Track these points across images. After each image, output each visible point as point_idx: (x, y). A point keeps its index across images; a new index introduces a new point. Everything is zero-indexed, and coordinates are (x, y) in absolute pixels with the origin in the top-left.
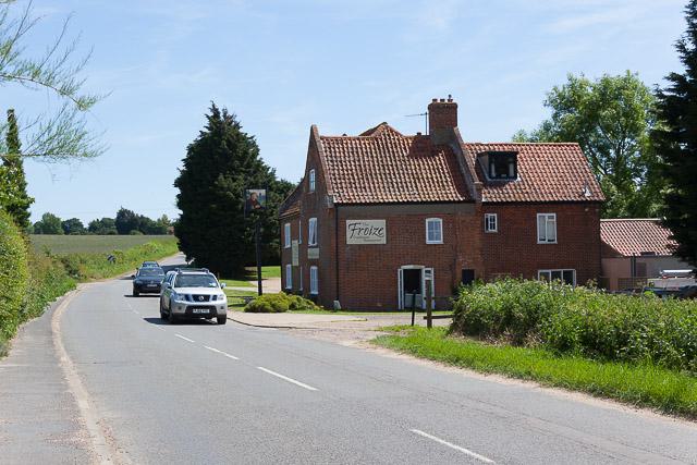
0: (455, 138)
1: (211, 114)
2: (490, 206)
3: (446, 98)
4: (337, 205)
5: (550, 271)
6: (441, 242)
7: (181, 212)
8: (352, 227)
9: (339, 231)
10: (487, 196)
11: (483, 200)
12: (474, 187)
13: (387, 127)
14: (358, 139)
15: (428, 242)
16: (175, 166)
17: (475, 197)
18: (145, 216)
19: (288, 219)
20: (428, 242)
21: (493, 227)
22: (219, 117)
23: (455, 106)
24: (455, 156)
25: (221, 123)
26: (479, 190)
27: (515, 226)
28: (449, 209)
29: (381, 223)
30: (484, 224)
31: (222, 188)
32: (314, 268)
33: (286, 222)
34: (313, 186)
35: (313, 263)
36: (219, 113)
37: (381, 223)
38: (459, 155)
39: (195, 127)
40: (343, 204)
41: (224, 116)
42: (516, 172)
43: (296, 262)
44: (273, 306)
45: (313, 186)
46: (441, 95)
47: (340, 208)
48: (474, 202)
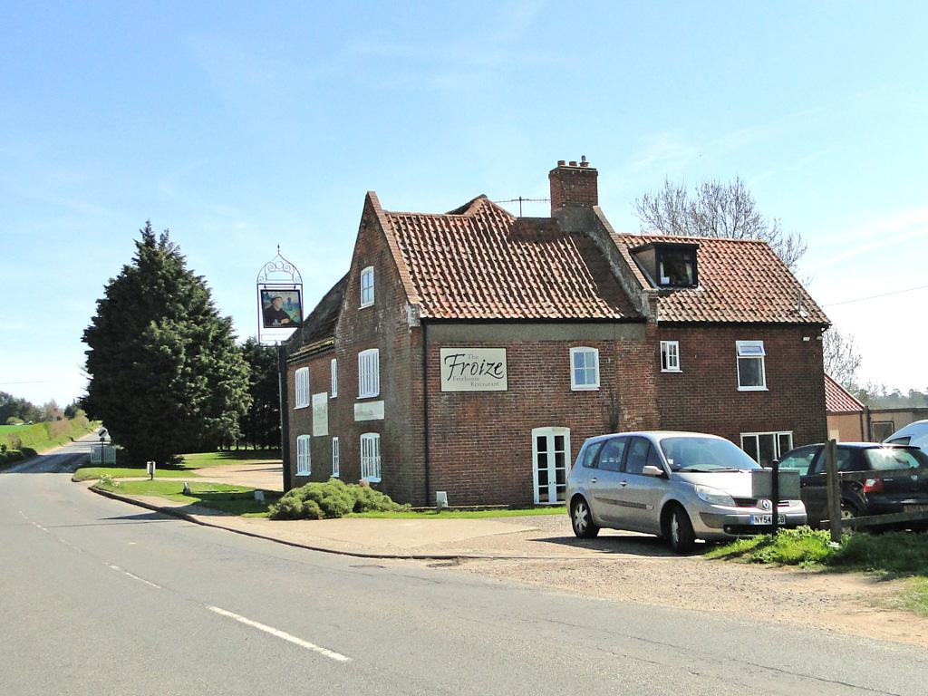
0: (597, 223)
1: (142, 241)
2: (669, 328)
3: (579, 161)
4: (424, 322)
5: (757, 435)
6: (595, 386)
7: (91, 377)
8: (450, 361)
9: (428, 369)
10: (666, 311)
11: (660, 319)
12: (644, 298)
13: (488, 203)
14: (445, 218)
15: (574, 387)
16: (86, 314)
17: (646, 312)
18: (27, 400)
19: (303, 360)
20: (574, 387)
21: (673, 363)
22: (153, 246)
23: (593, 175)
24: (599, 251)
25: (156, 254)
26: (653, 301)
27: (706, 362)
28: (606, 332)
29: (499, 355)
30: (660, 359)
31: (153, 341)
32: (372, 437)
33: (299, 366)
34: (368, 298)
35: (370, 426)
36: (153, 242)
37: (499, 355)
38: (607, 250)
39: (124, 257)
40: (435, 321)
41: (162, 245)
42: (695, 273)
43: (320, 427)
44: (323, 507)
45: (368, 298)
46: (571, 156)
47: (432, 328)
48: (642, 320)
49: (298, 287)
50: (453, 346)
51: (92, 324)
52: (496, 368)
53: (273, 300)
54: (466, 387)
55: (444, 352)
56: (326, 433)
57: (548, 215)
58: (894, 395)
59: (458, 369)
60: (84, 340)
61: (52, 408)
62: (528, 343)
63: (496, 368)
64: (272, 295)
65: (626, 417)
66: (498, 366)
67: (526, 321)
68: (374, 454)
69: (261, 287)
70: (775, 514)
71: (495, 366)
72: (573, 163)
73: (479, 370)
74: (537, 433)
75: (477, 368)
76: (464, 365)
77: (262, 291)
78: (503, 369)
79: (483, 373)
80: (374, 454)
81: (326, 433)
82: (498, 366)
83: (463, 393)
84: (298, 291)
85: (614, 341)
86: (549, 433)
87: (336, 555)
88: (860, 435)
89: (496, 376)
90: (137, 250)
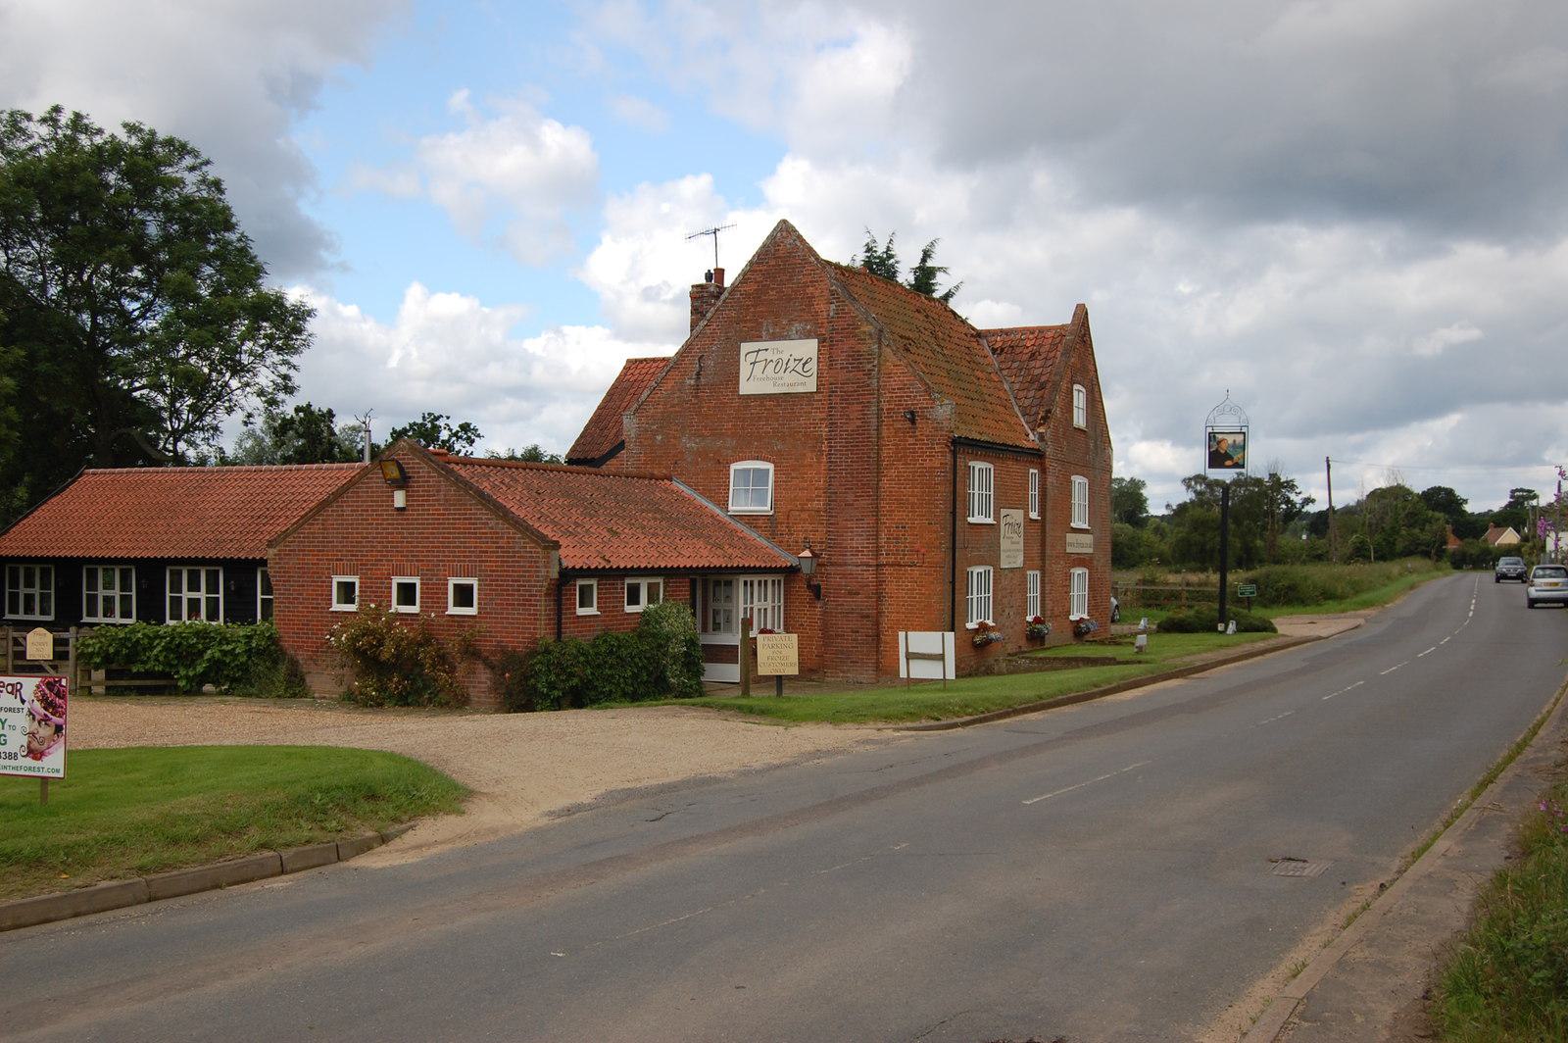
8: (752, 358)
43: (1012, 552)
49: (1244, 430)
51: (1188, 501)
52: (804, 365)
53: (1219, 443)
56: (1019, 562)
58: (447, 762)
59: (759, 367)
63: (804, 365)
64: (1219, 437)
66: (806, 363)
68: (975, 600)
69: (1210, 430)
70: (155, 296)
71: (803, 362)
73: (784, 367)
75: (783, 366)
76: (767, 362)
77: (1210, 433)
78: (813, 366)
79: (789, 370)
80: (975, 600)
81: (1019, 562)
82: (806, 363)
84: (1244, 433)
88: (947, 618)
89: (804, 373)
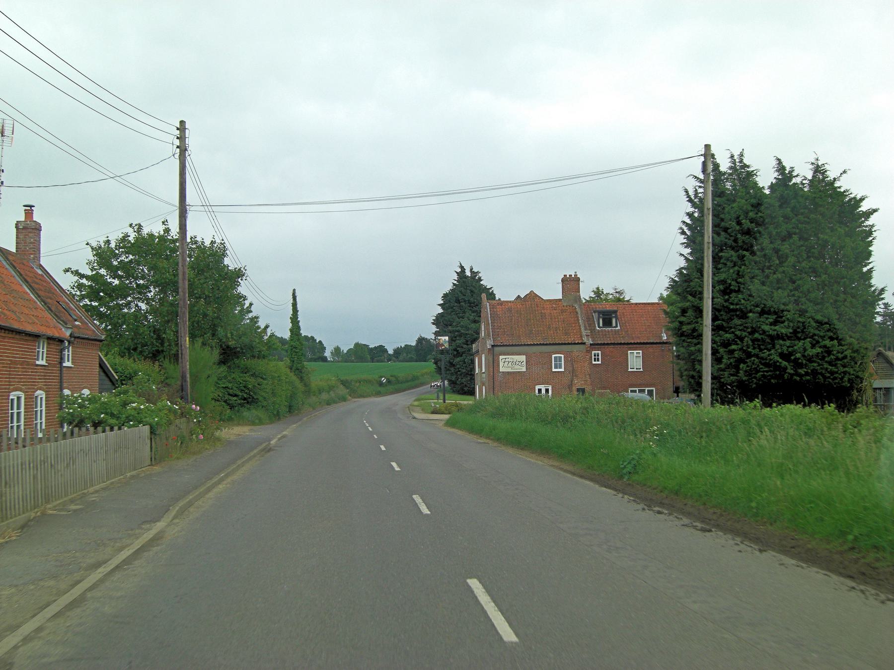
40: (497, 346)
46: (570, 272)
47: (496, 349)
50: (504, 355)
53: (439, 340)
54: (510, 370)
55: (501, 357)
57: (559, 296)
60: (394, 350)
61: (381, 349)
62: (535, 353)
65: (576, 382)
67: (534, 345)
72: (570, 275)
74: (537, 387)
83: (508, 372)
85: (572, 352)
86: (543, 388)
87: (239, 207)
90: (858, 197)
